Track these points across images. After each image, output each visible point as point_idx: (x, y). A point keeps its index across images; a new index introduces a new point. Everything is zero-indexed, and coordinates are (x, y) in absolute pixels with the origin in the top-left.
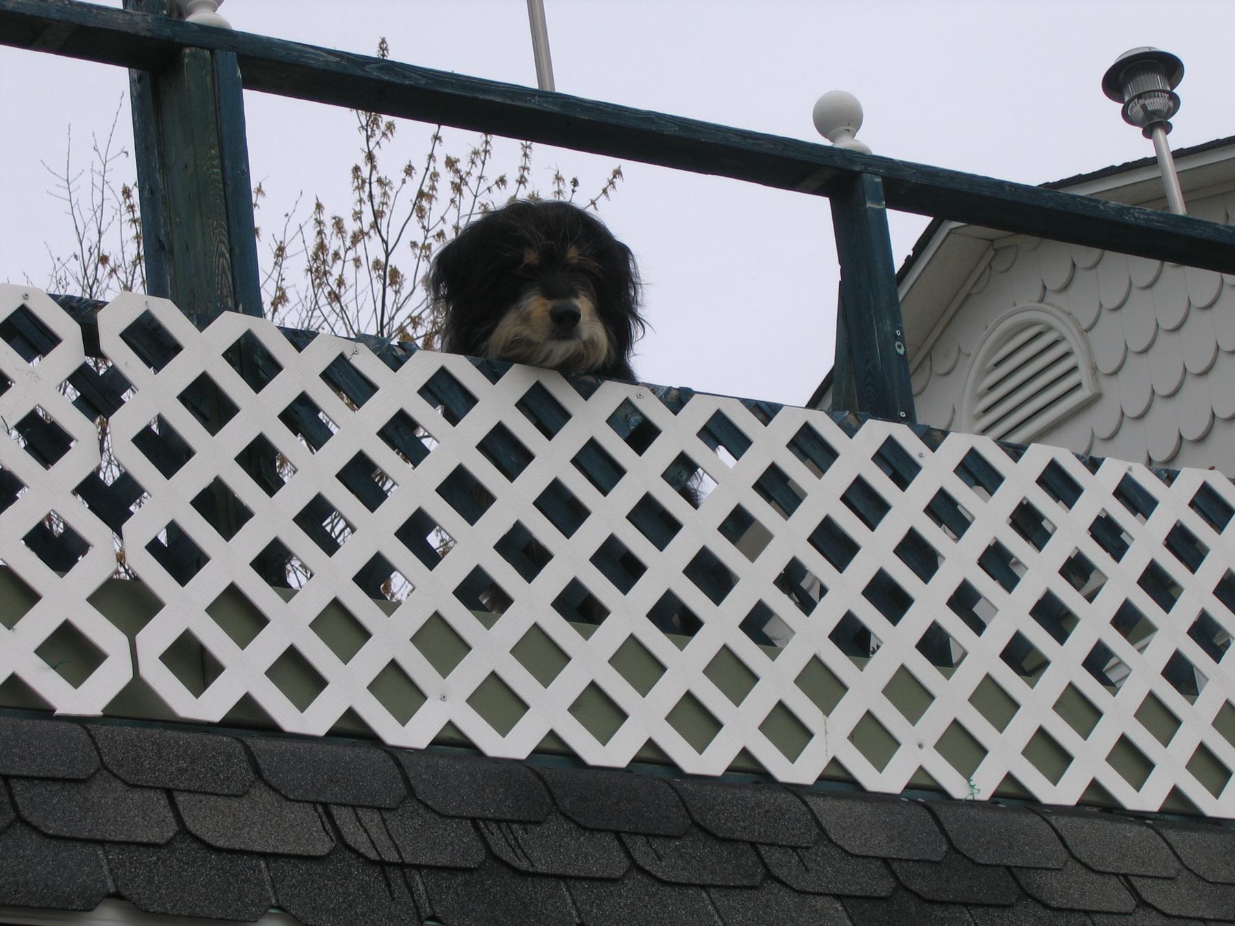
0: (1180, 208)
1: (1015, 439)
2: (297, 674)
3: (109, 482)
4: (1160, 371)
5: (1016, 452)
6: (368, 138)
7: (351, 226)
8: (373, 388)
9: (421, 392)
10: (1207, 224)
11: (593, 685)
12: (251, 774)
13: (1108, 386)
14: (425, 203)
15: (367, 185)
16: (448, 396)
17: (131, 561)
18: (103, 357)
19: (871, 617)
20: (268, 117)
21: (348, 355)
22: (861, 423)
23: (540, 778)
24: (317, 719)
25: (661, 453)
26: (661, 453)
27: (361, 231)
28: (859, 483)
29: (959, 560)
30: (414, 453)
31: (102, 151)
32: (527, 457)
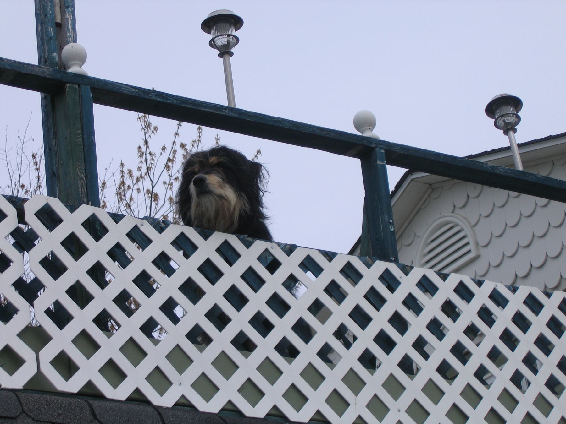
0: (520, 167)
1: (445, 271)
2: (112, 371)
3: (28, 282)
4: (507, 245)
5: (444, 277)
6: (145, 133)
7: (136, 174)
8: (150, 241)
9: (172, 243)
10: (532, 174)
11: (249, 380)
12: (92, 416)
13: (483, 252)
14: (170, 164)
15: (144, 155)
16: (184, 245)
17: (37, 317)
18: (26, 224)
19: (377, 351)
20: (104, 117)
21: (139, 226)
22: (374, 262)
23: (225, 421)
24: (122, 393)
25: (282, 274)
26: (282, 274)
27: (141, 176)
28: (372, 289)
29: (418, 326)
30: (169, 271)
31: (22, 138)
32: (220, 274)
